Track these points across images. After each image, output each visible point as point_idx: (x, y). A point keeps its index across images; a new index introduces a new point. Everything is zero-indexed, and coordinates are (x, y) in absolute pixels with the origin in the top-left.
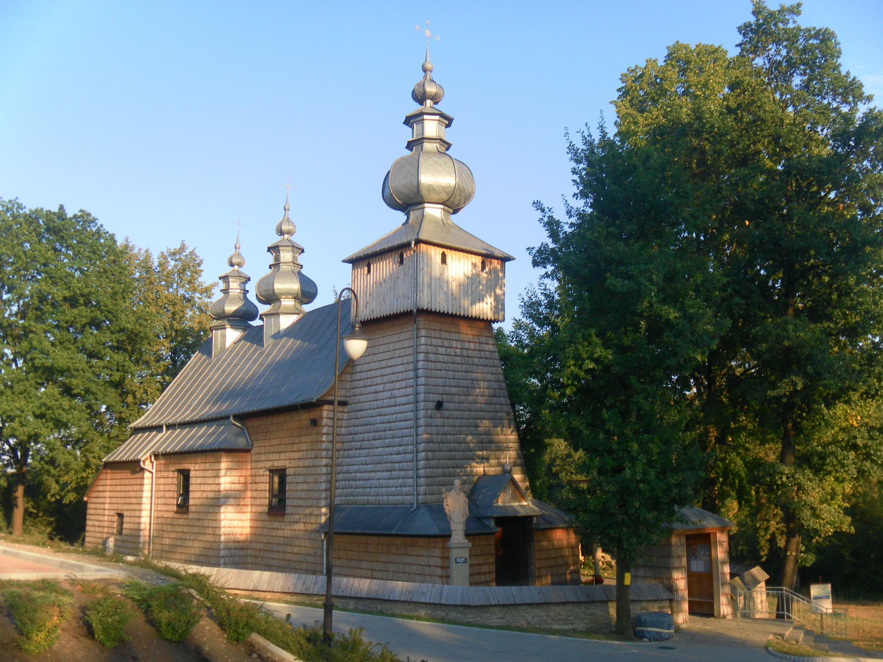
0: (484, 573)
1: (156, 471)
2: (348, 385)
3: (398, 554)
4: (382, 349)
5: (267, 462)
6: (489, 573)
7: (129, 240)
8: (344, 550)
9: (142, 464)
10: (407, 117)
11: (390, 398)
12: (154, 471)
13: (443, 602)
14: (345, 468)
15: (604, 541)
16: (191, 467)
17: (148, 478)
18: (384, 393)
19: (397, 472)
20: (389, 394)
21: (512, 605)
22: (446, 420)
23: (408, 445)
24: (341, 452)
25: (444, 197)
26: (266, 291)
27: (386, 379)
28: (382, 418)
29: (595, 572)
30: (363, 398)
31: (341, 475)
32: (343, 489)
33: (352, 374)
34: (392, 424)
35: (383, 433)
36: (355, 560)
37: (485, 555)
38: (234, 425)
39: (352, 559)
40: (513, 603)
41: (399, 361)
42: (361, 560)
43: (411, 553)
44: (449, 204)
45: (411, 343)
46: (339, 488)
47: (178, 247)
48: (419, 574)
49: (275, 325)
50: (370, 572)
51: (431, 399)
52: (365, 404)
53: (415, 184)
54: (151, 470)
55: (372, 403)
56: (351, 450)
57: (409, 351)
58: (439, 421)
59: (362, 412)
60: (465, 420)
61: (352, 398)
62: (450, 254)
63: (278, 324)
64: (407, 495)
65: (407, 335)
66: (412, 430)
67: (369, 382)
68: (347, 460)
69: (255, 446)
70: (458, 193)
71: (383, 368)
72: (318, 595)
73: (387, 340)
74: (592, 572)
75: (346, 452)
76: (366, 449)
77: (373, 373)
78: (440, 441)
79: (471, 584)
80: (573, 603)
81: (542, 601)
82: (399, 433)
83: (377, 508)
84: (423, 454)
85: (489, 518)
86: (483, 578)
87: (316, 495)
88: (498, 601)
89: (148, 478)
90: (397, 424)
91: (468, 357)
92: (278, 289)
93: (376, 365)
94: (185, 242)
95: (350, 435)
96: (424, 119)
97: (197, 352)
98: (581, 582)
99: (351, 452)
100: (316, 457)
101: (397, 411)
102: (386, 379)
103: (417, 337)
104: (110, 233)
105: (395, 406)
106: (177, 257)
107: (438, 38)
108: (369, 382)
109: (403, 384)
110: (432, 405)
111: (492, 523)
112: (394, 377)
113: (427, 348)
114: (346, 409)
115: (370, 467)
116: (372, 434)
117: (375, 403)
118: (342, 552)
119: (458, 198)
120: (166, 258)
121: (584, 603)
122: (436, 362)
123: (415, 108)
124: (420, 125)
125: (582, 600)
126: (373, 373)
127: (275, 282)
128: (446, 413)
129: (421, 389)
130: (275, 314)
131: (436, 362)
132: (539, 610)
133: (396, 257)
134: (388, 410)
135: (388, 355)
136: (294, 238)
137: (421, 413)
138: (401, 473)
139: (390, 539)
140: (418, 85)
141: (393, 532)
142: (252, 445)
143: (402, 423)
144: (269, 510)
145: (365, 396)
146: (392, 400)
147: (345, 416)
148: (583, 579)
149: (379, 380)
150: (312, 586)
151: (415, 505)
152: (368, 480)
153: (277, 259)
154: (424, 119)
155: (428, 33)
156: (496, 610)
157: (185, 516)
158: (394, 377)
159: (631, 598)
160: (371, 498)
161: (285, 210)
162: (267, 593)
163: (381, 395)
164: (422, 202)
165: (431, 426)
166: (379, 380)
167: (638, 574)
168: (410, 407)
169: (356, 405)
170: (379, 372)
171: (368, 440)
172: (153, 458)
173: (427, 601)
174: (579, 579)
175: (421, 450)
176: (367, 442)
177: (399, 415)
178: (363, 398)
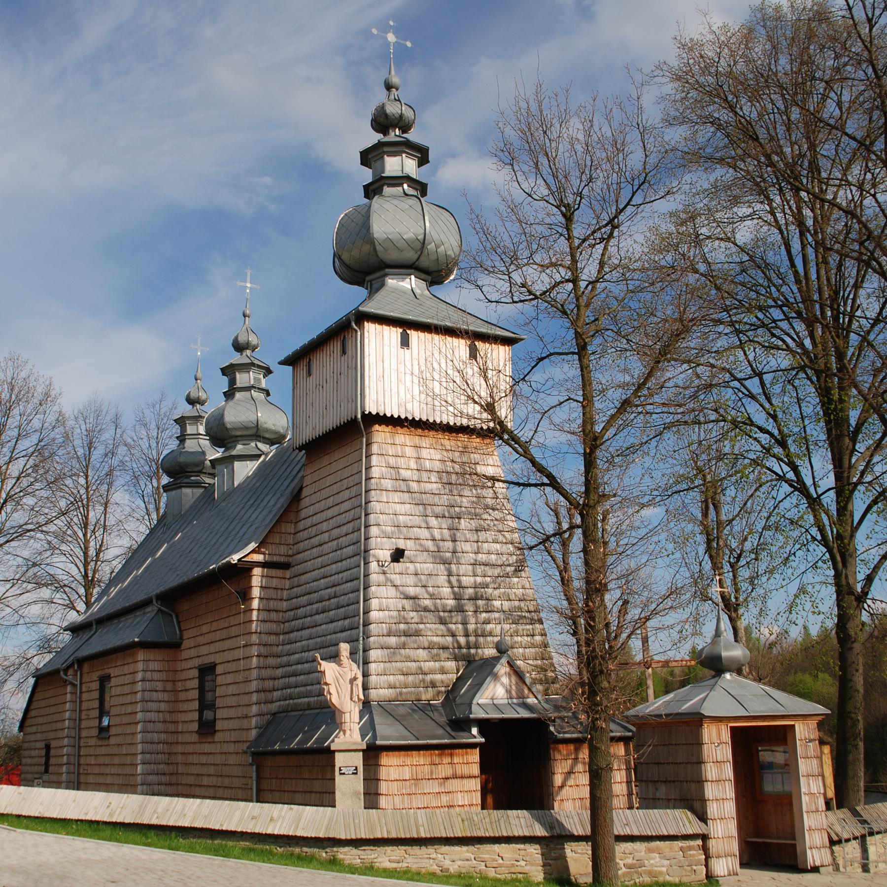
8: (276, 778)
9: (62, 673)
24: (281, 637)
27: (332, 523)
32: (282, 689)
34: (338, 588)
46: (278, 690)
52: (309, 563)
56: (292, 632)
61: (295, 557)
68: (288, 647)
75: (287, 636)
77: (316, 519)
79: (365, 808)
87: (245, 700)
88: (388, 832)
93: (322, 505)
95: (291, 610)
99: (292, 635)
101: (344, 568)
102: (332, 523)
105: (342, 561)
108: (313, 531)
114: (288, 574)
117: (320, 559)
123: (376, 137)
126: (316, 519)
130: (228, 460)
142: (181, 638)
143: (349, 584)
144: (199, 728)
146: (338, 552)
147: (287, 584)
150: (119, 809)
153: (232, 382)
159: (619, 830)
160: (312, 699)
171: (311, 616)
177: (345, 573)
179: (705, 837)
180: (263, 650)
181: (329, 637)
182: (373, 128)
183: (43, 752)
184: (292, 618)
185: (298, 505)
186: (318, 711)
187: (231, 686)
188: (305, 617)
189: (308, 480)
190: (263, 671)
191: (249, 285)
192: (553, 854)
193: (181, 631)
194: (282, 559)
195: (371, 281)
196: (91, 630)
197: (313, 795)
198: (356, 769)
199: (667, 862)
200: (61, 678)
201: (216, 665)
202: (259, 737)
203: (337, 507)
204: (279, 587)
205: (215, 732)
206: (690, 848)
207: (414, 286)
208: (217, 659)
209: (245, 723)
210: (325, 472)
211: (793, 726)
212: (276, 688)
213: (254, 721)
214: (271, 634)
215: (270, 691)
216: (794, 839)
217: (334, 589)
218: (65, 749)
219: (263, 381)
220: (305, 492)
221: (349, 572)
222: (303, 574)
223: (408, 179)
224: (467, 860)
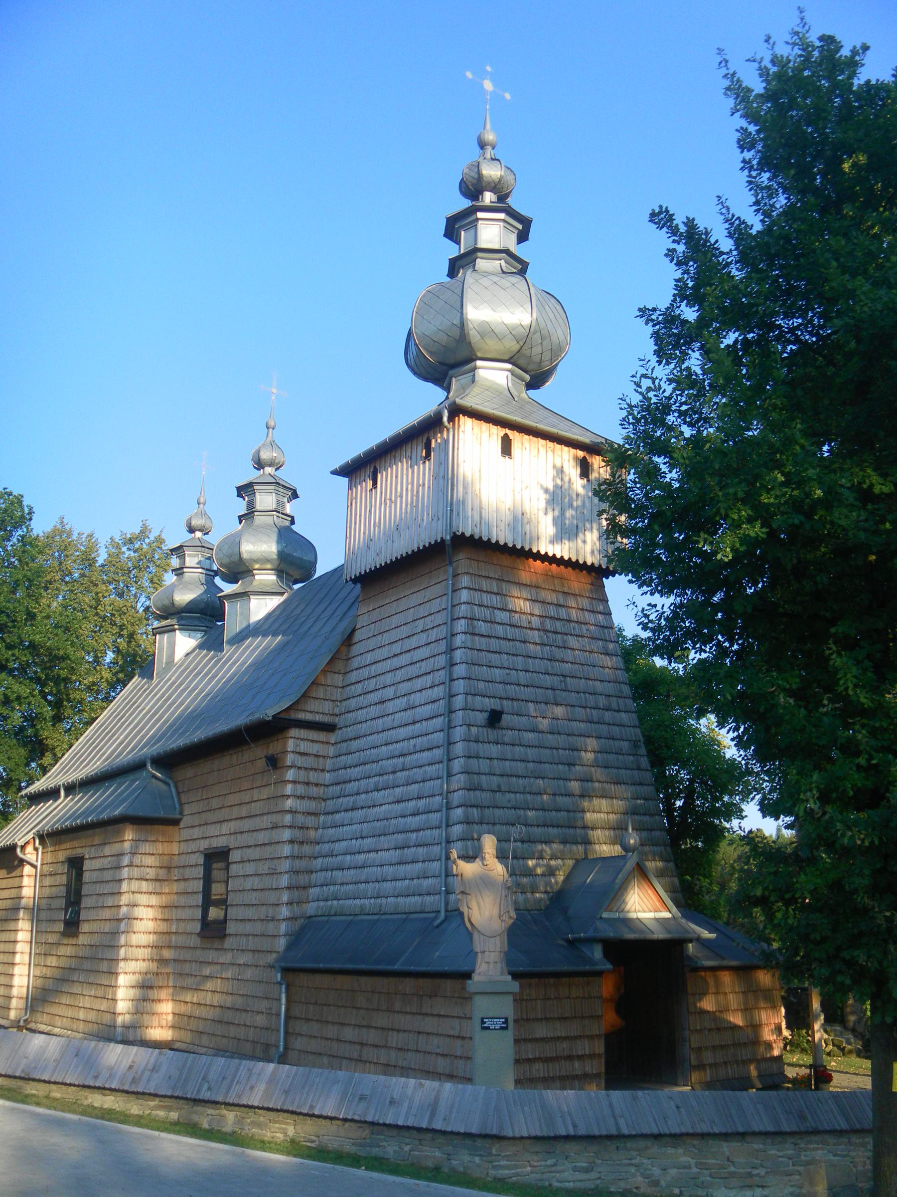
0: (581, 1057)
1: (42, 864)
2: (337, 694)
3: (406, 1013)
4: (395, 621)
5: (202, 841)
6: (592, 1056)
7: (65, 521)
8: (316, 1003)
9: (18, 850)
10: (448, 219)
11: (405, 710)
12: (39, 864)
13: (438, 1125)
14: (326, 847)
15: (839, 978)
16: (86, 852)
17: (29, 876)
18: (397, 701)
19: (413, 850)
20: (402, 702)
21: (609, 1137)
22: (509, 748)
23: (433, 796)
24: (322, 818)
25: (513, 346)
26: (229, 557)
27: (400, 675)
28: (391, 747)
29: (815, 1058)
30: (360, 715)
31: (320, 860)
32: (322, 886)
33: (345, 673)
34: (408, 758)
35: (391, 776)
36: (333, 1023)
37: (583, 1017)
38: (154, 776)
39: (327, 1022)
40: (614, 1131)
41: (423, 638)
42: (342, 1024)
43: (429, 1012)
44: (522, 362)
45: (444, 602)
46: (315, 886)
47: (137, 531)
48: (443, 1055)
49: (241, 614)
50: (358, 1047)
51: (478, 706)
52: (364, 725)
53: (457, 321)
54: (35, 863)
55: (375, 722)
56: (338, 812)
57: (440, 618)
58: (494, 750)
59: (358, 741)
60: (548, 751)
61: (343, 717)
62: (519, 440)
63: (247, 613)
64: (429, 894)
65: (438, 590)
66: (441, 765)
67: (371, 685)
68: (331, 831)
69: (186, 813)
70: (537, 338)
71: (395, 656)
72: (156, 1095)
73: (403, 604)
74: (808, 1060)
76: (362, 808)
77: (374, 670)
78: (495, 788)
80: (766, 1134)
81: (687, 1128)
82: (418, 773)
83: (377, 921)
84: (459, 811)
85: (591, 941)
86: (577, 1067)
87: (272, 897)
88: (575, 1126)
89: (29, 876)
90: (414, 757)
91: (556, 633)
92: (246, 552)
93: (384, 652)
94: (148, 523)
95: (337, 784)
96: (477, 219)
97: (136, 677)
98: (787, 1080)
99: (337, 816)
100: (275, 827)
101: (416, 733)
102: (400, 675)
103: (453, 591)
104: (15, 493)
105: (414, 723)
106: (137, 545)
107: (508, 96)
108: (371, 685)
109: (428, 680)
110: (481, 718)
111: (598, 953)
112: (414, 670)
113: (472, 611)
114: (333, 738)
115: (368, 843)
116: (373, 780)
117: (380, 721)
118: (311, 1007)
119: (537, 350)
120: (118, 547)
121: (792, 1134)
122: (489, 637)
124: (472, 231)
125: (786, 1128)
126: (374, 670)
127: (243, 541)
128: (509, 735)
129: (460, 686)
131: (489, 637)
132: (680, 1151)
133: (419, 448)
134: (402, 732)
135: (404, 631)
136: (281, 474)
137: (459, 733)
138: (420, 850)
139: (392, 980)
140: (472, 165)
141: (396, 967)
142: (181, 813)
143: (426, 754)
144: (202, 929)
145: (364, 711)
146: (409, 712)
147: (331, 751)
148: (791, 1072)
149: (388, 679)
151: (443, 914)
152: (363, 867)
153: (251, 506)
154: (477, 219)
155: (488, 85)
156: (572, 1148)
157: (73, 941)
158: (414, 670)
160: (367, 901)
161: (268, 428)
162: (54, 1087)
163: (390, 707)
164: (472, 359)
165: (478, 757)
166: (388, 679)
168: (438, 722)
169: (349, 729)
170: (388, 665)
171: (367, 792)
172: (37, 841)
173: (400, 1123)
174: (782, 1073)
175: (455, 803)
176: (364, 796)
178: (360, 715)
180: (298, 834)
181: (393, 821)
182: (460, 189)
184: (338, 793)
185: (349, 651)
186: (376, 917)
187: (251, 878)
188: (358, 794)
189: (361, 622)
190: (297, 862)
192: (803, 1158)
193: (181, 805)
194: (326, 719)
196: (55, 801)
197: (372, 1031)
198: (506, 1022)
200: (17, 857)
201: (229, 850)
202: (289, 948)
203: (408, 655)
204: (321, 753)
205: (225, 936)
207: (510, 385)
208: (232, 842)
209: (271, 928)
210: (394, 608)
212: (313, 884)
213: (283, 927)
214: (309, 813)
215: (304, 888)
217: (401, 759)
219: (288, 506)
220: (358, 636)
221: (425, 739)
222: (355, 739)
223: (507, 252)
224: (684, 1167)
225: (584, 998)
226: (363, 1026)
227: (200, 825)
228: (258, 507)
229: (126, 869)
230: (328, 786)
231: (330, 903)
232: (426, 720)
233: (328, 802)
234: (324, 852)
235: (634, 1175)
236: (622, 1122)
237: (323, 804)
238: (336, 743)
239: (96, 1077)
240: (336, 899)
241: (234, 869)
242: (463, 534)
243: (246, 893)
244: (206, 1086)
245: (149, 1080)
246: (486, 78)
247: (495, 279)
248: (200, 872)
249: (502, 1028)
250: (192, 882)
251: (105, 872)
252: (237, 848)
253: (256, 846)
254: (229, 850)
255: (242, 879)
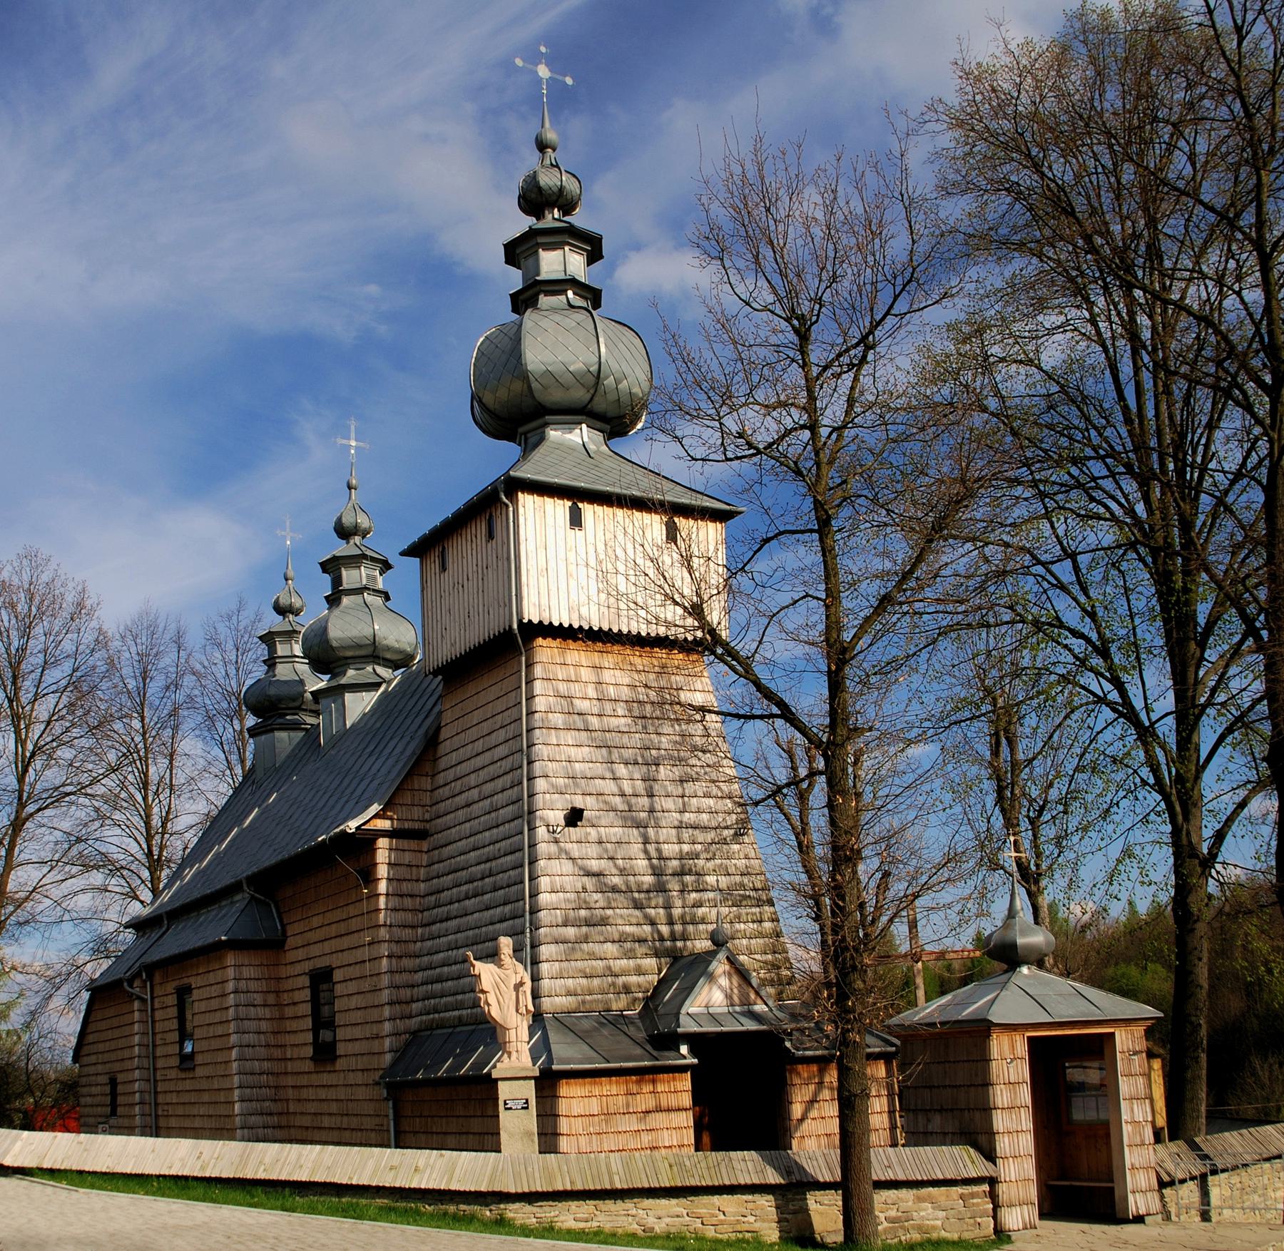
8: (421, 1116)
9: (125, 984)
11: (489, 813)
18: (481, 804)
24: (420, 930)
34: (494, 863)
35: (480, 883)
39: (432, 1133)
52: (453, 830)
55: (463, 826)
56: (434, 923)
61: (433, 822)
68: (429, 943)
76: (456, 917)
87: (374, 1014)
93: (468, 751)
95: (432, 894)
99: (435, 928)
114: (425, 846)
117: (468, 825)
123: (525, 223)
130: (336, 692)
143: (509, 858)
149: (473, 780)
152: (459, 978)
159: (878, 1174)
160: (464, 1012)
167: (930, 1128)
171: (459, 901)
176: (457, 904)
179: (993, 1181)
181: (484, 929)
183: (108, 1089)
188: (451, 903)
189: (447, 717)
190: (397, 976)
191: (353, 443)
192: (791, 1207)
194: (417, 826)
195: (525, 434)
198: (527, 1102)
199: (942, 1214)
201: (333, 969)
202: (395, 1063)
206: (973, 1195)
207: (586, 439)
208: (335, 961)
209: (375, 1046)
211: (1113, 1034)
213: (387, 1042)
215: (407, 1003)
216: (1112, 1181)
217: (488, 865)
218: (137, 1084)
219: (380, 579)
220: (444, 734)
221: (509, 841)
223: (573, 283)
224: (678, 1216)
225: (670, 1092)
226: (463, 1133)
227: (303, 946)
228: (346, 585)
229: (232, 996)
230: (423, 897)
231: (431, 1016)
232: (509, 822)
233: (425, 913)
234: (424, 966)
235: (631, 1224)
236: (616, 1178)
237: (420, 915)
238: (428, 851)
239: (170, 1167)
240: (437, 1011)
241: (339, 989)
242: (530, 621)
243: (351, 1012)
244: (262, 1168)
245: (214, 1166)
246: (540, 63)
247: (557, 318)
248: (306, 994)
249: (523, 1108)
250: (301, 1005)
251: (213, 1000)
252: (339, 967)
253: (356, 963)
254: (333, 969)
255: (346, 998)
